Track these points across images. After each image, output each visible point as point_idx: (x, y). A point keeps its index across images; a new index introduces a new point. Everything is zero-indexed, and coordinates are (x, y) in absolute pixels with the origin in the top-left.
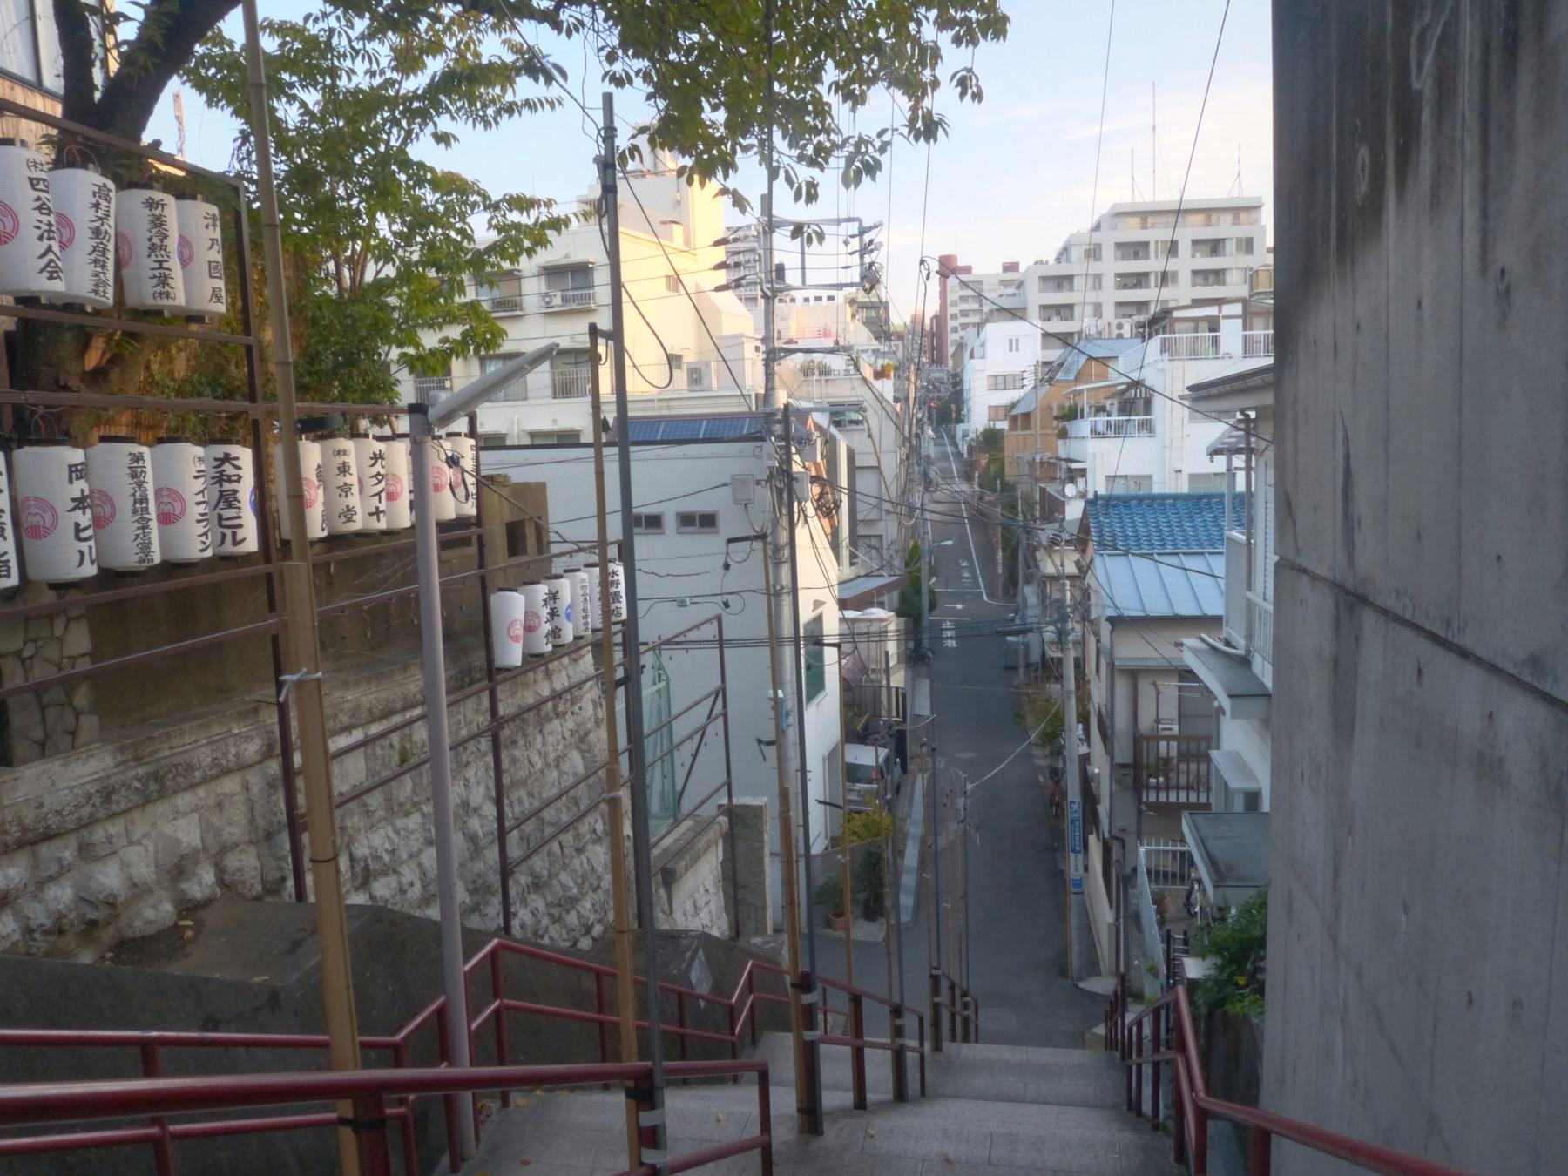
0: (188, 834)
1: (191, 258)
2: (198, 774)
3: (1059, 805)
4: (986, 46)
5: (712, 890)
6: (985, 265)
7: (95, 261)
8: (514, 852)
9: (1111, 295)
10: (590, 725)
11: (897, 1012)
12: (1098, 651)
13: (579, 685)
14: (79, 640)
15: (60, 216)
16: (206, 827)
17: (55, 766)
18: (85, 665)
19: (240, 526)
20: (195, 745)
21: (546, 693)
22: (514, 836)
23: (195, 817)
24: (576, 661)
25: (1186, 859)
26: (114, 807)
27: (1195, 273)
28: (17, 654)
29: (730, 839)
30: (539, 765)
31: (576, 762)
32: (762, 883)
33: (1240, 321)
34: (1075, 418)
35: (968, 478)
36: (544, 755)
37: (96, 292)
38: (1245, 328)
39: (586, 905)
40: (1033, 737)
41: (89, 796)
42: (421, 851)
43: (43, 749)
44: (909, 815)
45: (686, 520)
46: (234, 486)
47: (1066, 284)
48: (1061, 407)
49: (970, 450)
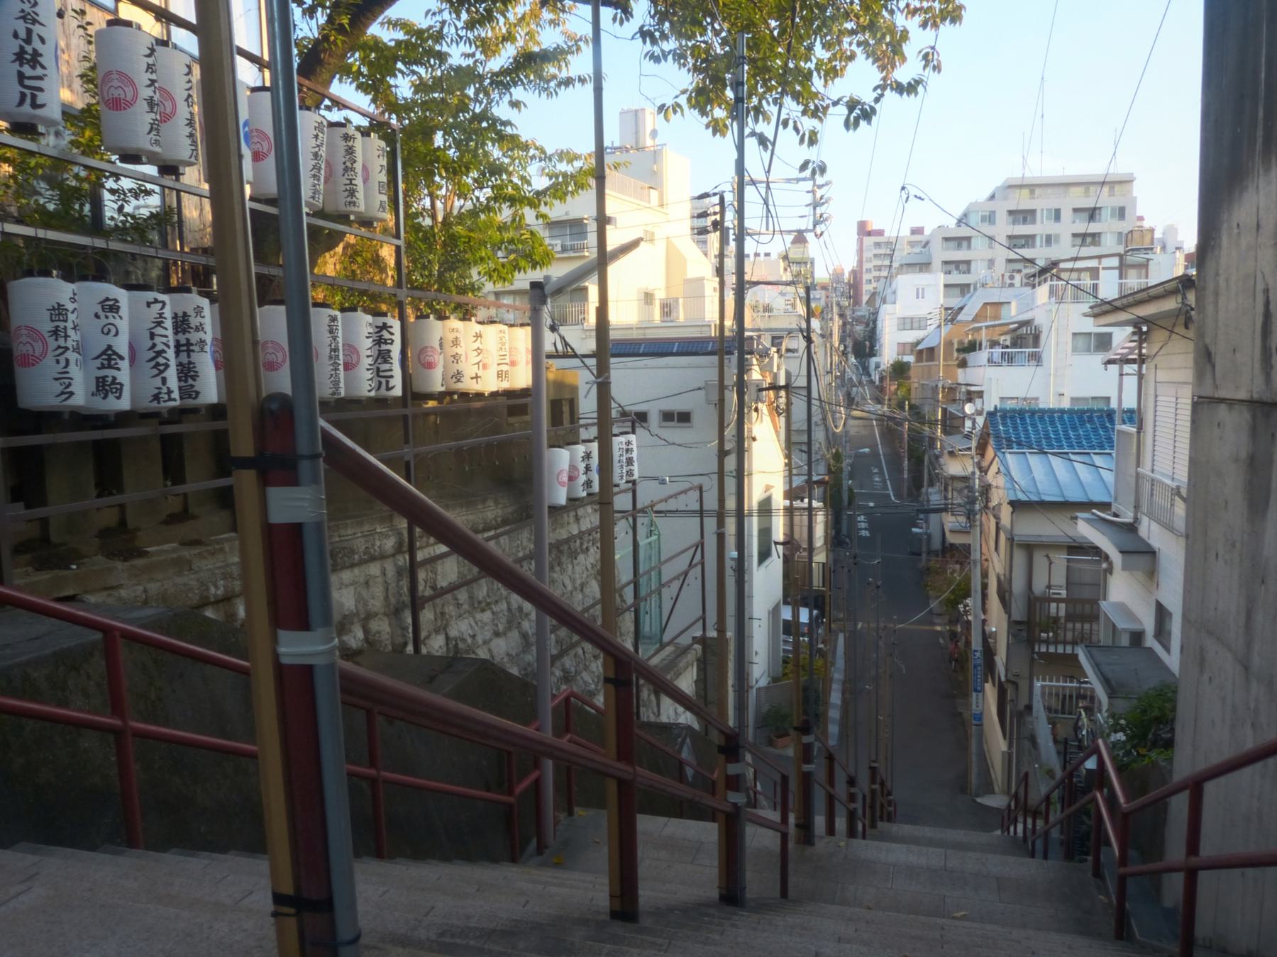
2: (356, 557)
4: (946, 28)
7: (314, 176)
16: (359, 599)
23: (352, 589)
27: (1075, 235)
29: (703, 664)
30: (570, 588)
33: (1117, 272)
34: (974, 350)
35: (879, 401)
36: (573, 581)
38: (1121, 278)
40: (934, 604)
42: (491, 640)
44: (833, 664)
45: (667, 416)
46: (388, 347)
47: (965, 244)
48: (961, 342)
49: (882, 379)
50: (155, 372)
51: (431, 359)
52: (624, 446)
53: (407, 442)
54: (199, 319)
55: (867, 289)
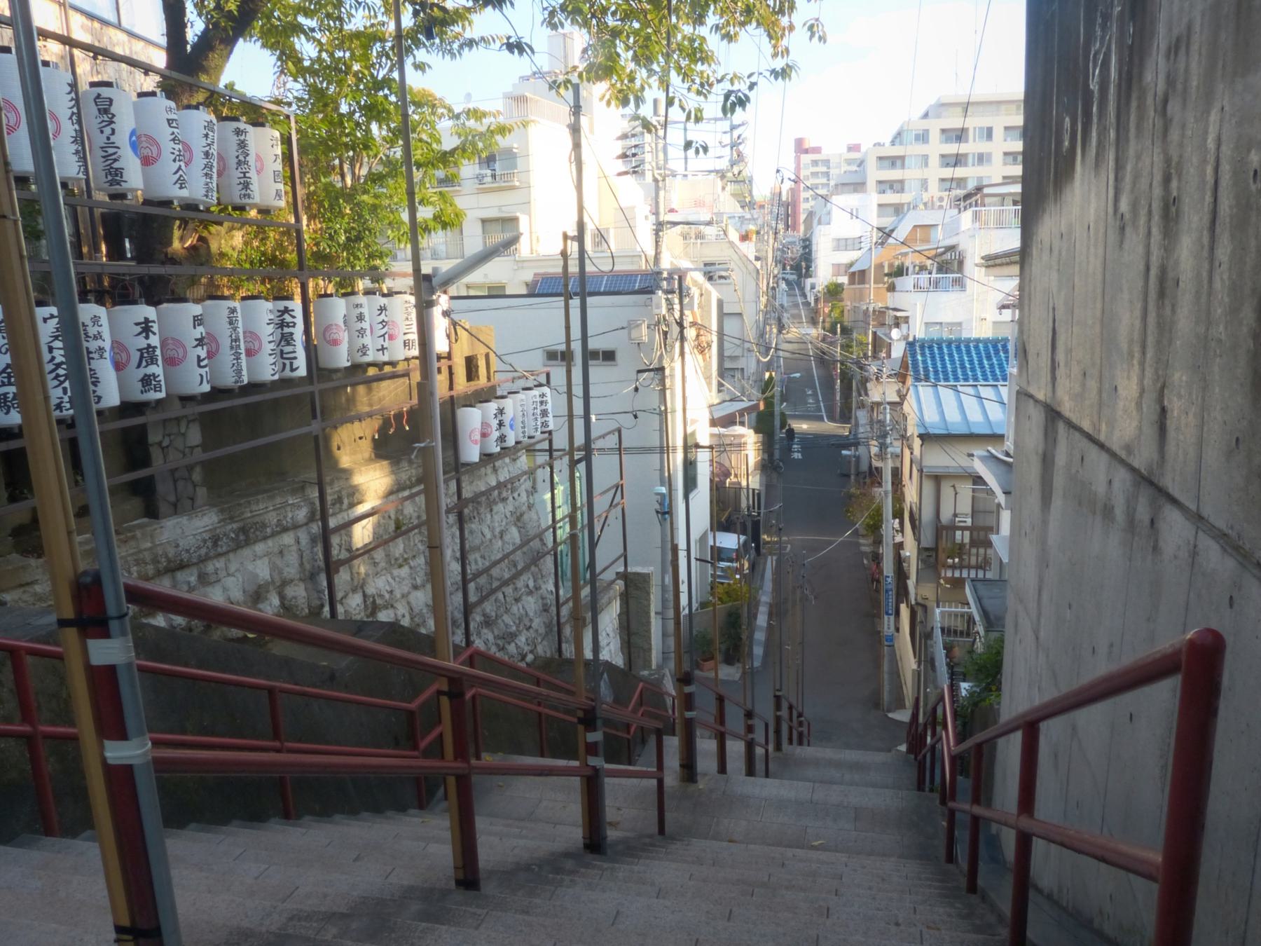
0: (263, 571)
1: (262, 169)
2: (269, 530)
3: (878, 581)
5: (612, 635)
6: (834, 148)
7: (206, 175)
8: (473, 598)
9: (936, 172)
10: (524, 508)
11: (749, 715)
12: (911, 461)
13: (518, 478)
14: (195, 435)
15: (184, 144)
16: (274, 567)
17: (184, 520)
18: (199, 455)
19: (295, 358)
20: (266, 510)
21: (494, 483)
22: (472, 586)
23: (266, 560)
24: (514, 460)
25: (970, 620)
26: (219, 550)
27: (1006, 154)
28: (160, 444)
29: (625, 597)
30: (489, 536)
31: (514, 535)
32: (649, 631)
35: (814, 322)
36: (492, 529)
37: (207, 196)
39: (522, 640)
41: (205, 541)
42: (409, 593)
43: (176, 509)
44: (761, 587)
46: (291, 330)
47: (899, 163)
49: (817, 300)
50: (56, 383)
51: (335, 336)
52: (538, 399)
53: (315, 417)
54: (96, 328)
55: (804, 207)
